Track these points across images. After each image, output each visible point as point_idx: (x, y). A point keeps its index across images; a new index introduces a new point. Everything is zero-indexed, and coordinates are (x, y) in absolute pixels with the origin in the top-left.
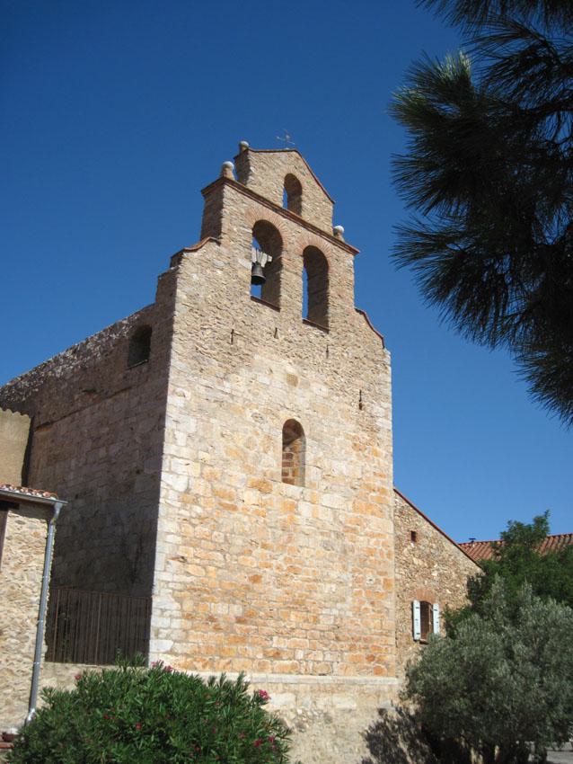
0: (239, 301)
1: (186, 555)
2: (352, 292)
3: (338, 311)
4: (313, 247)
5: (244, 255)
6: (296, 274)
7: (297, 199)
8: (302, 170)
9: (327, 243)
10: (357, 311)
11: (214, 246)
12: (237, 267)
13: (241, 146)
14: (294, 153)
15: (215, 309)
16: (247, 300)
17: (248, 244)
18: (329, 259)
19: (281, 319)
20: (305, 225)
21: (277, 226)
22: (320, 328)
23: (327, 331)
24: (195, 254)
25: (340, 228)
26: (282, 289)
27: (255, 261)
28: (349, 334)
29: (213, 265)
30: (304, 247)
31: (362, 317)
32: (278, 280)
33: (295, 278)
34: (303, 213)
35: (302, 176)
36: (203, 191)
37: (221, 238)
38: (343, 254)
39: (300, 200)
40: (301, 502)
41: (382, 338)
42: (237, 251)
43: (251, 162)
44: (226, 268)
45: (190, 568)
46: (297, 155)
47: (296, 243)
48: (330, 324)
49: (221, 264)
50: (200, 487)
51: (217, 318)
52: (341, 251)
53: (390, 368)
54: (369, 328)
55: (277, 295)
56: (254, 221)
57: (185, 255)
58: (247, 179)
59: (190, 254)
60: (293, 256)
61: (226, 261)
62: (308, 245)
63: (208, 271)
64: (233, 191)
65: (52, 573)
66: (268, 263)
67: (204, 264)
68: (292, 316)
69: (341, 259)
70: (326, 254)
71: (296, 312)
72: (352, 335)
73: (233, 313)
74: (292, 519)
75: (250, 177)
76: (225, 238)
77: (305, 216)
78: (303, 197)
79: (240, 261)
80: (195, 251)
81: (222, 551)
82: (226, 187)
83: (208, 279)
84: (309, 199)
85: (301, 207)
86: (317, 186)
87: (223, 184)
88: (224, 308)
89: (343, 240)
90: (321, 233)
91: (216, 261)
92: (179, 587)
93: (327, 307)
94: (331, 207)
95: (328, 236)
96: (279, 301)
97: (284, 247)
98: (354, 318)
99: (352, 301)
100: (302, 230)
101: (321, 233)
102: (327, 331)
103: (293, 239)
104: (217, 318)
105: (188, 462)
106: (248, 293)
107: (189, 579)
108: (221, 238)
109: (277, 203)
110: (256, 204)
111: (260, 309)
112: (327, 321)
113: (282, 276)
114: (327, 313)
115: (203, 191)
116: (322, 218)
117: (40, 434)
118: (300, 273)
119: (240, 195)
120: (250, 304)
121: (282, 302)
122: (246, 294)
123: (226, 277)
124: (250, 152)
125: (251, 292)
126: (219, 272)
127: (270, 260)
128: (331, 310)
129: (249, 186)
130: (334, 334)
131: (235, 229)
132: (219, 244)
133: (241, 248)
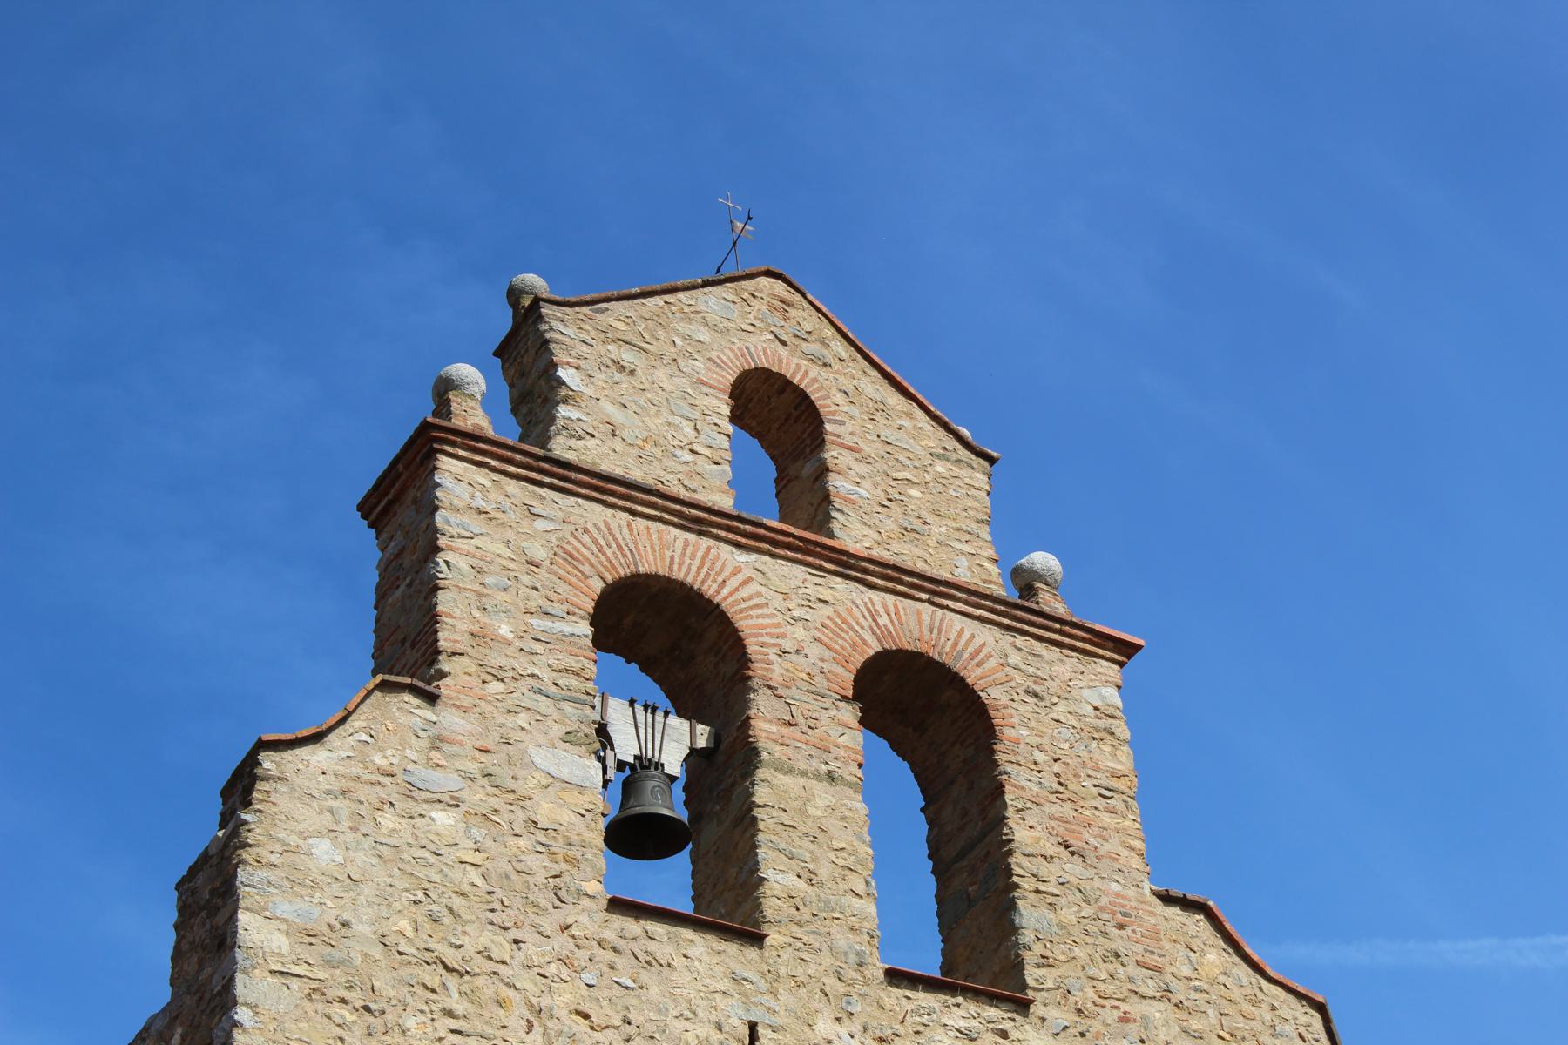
0: (548, 925)
2: (1131, 822)
3: (1068, 915)
4: (901, 652)
5: (558, 731)
6: (831, 777)
7: (808, 469)
8: (813, 348)
9: (972, 627)
10: (1167, 899)
11: (406, 710)
12: (526, 786)
13: (514, 294)
14: (764, 281)
15: (433, 976)
16: (591, 919)
17: (574, 682)
18: (993, 695)
19: (772, 976)
20: (848, 565)
21: (709, 590)
22: (994, 999)
23: (1022, 1006)
24: (316, 756)
25: (1042, 560)
26: (762, 853)
27: (626, 748)
28: (1135, 1008)
29: (411, 791)
30: (859, 660)
31: (1197, 925)
32: (746, 822)
33: (823, 795)
34: (838, 522)
35: (815, 371)
36: (365, 508)
37: (442, 675)
38: (1060, 666)
39: (823, 470)
41: (1321, 1008)
42: (522, 719)
43: (560, 355)
44: (476, 796)
46: (780, 288)
47: (814, 651)
48: (1032, 975)
49: (447, 781)
51: (449, 1013)
52: (1050, 653)
54: (1243, 972)
55: (749, 883)
56: (598, 586)
57: (268, 761)
58: (553, 419)
59: (288, 755)
60: (806, 704)
61: (473, 768)
62: (874, 647)
63: (388, 820)
64: (482, 477)
65: (805, 530)
66: (694, 757)
67: (363, 792)
68: (827, 960)
69: (1054, 686)
70: (972, 676)
71: (842, 940)
72: (1156, 1011)
73: (526, 982)
75: (563, 411)
76: (457, 675)
77: (851, 533)
78: (832, 455)
79: (541, 757)
80: (317, 738)
82: (444, 462)
83: (387, 852)
84: (865, 460)
85: (826, 499)
86: (894, 399)
87: (431, 455)
88: (479, 964)
89: (1061, 610)
90: (936, 589)
91: (422, 774)
93: (1012, 906)
94: (981, 479)
95: (974, 596)
96: (757, 906)
97: (757, 669)
98: (1155, 934)
99: (1136, 862)
100: (842, 590)
101: (936, 589)
102: (1022, 1006)
103: (799, 632)
104: (449, 1013)
106: (593, 887)
108: (442, 675)
109: (703, 497)
110: (596, 514)
111: (663, 950)
112: (1019, 966)
113: (761, 794)
114: (1015, 930)
115: (365, 508)
116: (939, 529)
117: (851, 533)
118: (851, 772)
119: (513, 487)
120: (609, 935)
121: (772, 906)
122: (581, 893)
123: (477, 833)
124: (546, 310)
125: (606, 881)
126: (443, 819)
127: (702, 743)
128: (1030, 916)
129: (561, 447)
130: (1059, 1016)
131: (505, 630)
132: (432, 699)
133: (544, 704)
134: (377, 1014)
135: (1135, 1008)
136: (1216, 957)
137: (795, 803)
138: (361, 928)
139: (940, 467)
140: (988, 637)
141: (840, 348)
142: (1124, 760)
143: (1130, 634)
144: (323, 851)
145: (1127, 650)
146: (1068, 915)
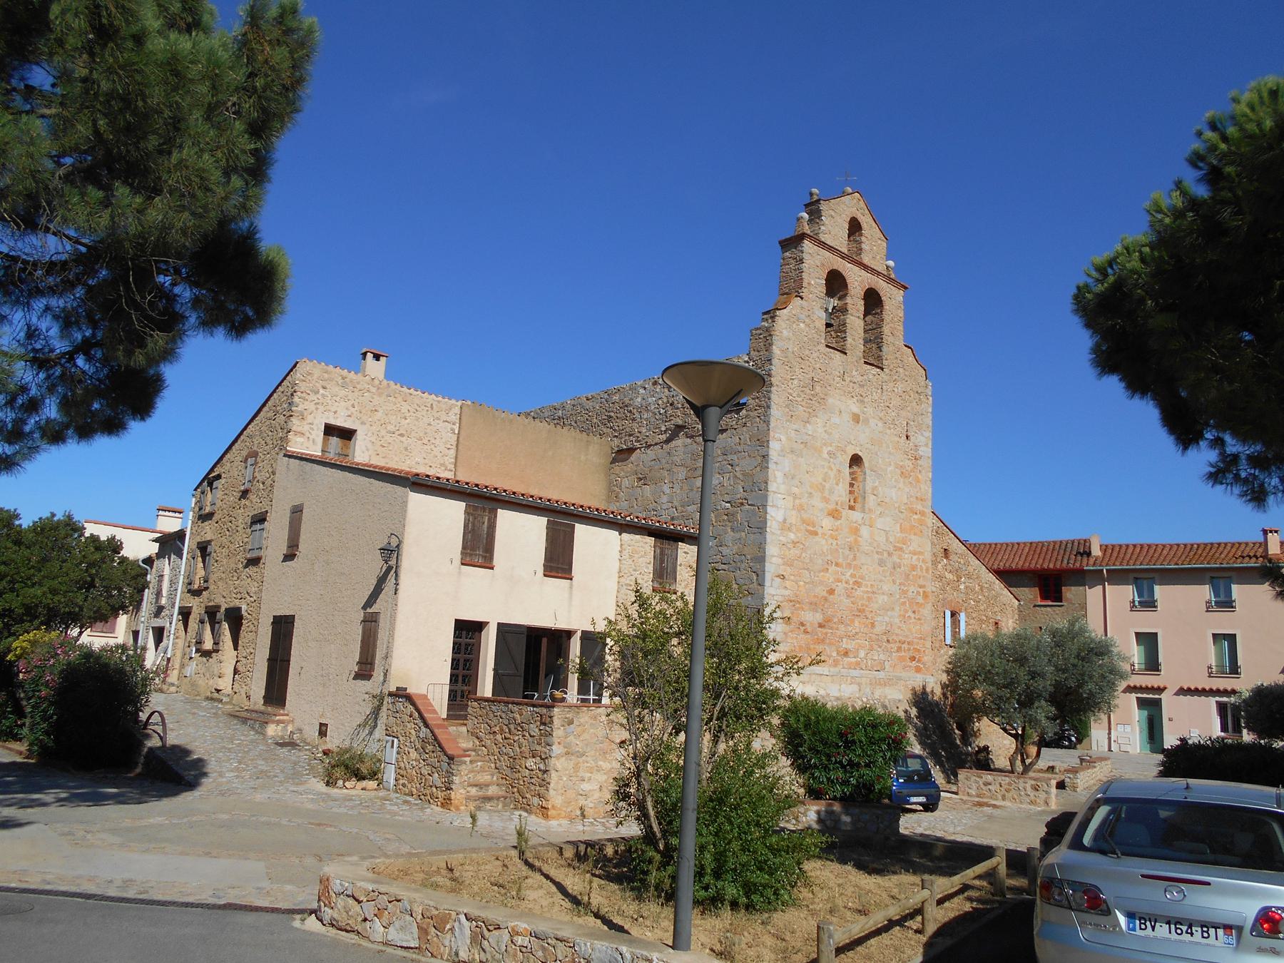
1: (784, 574)
10: (906, 346)
21: (843, 273)
28: (898, 369)
45: (788, 583)
50: (793, 518)
53: (931, 398)
77: (866, 259)
81: (808, 569)
87: (803, 239)
105: (784, 496)
107: (787, 593)
111: (833, 356)
126: (802, 325)
134: (205, 585)
135: (898, 369)
136: (911, 359)
137: (820, 430)
138: (790, 350)
139: (879, 242)
140: (884, 284)
141: (867, 212)
142: (902, 315)
143: (538, 674)
144: (785, 332)
145: (906, 288)
146: (891, 349)
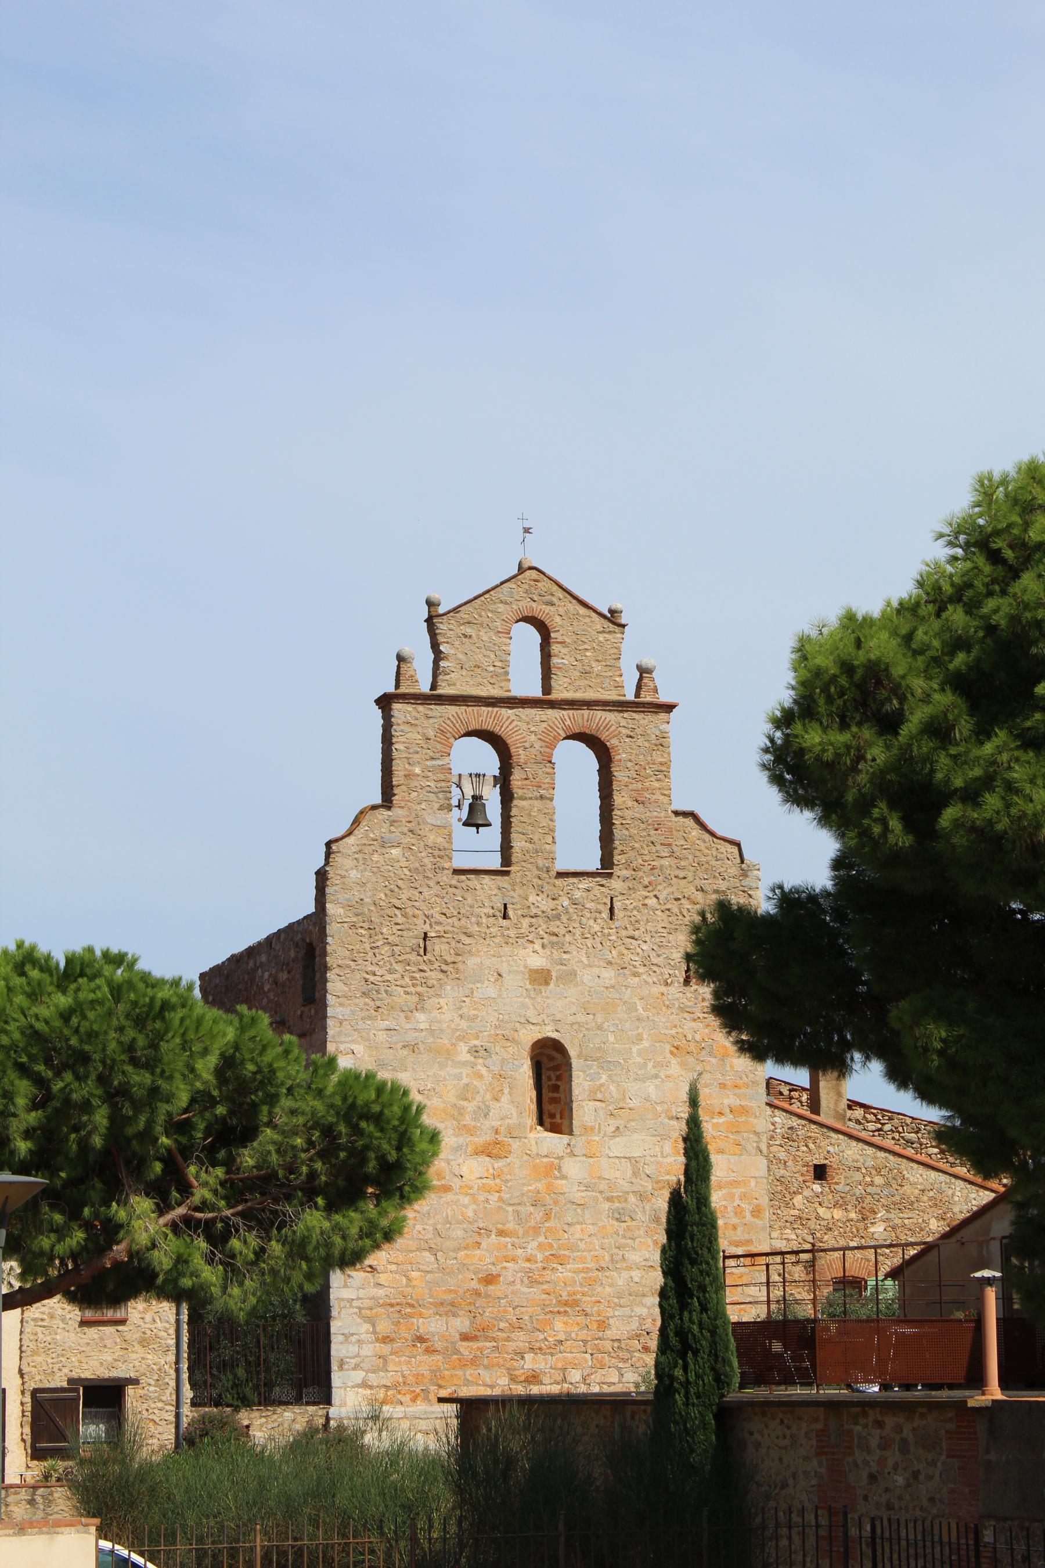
40: (566, 1159)
45: (383, 1278)
74: (549, 1186)
92: (367, 1303)
